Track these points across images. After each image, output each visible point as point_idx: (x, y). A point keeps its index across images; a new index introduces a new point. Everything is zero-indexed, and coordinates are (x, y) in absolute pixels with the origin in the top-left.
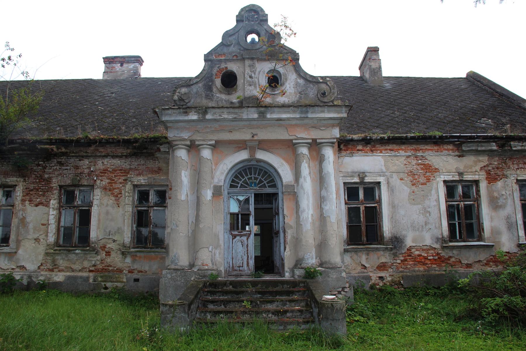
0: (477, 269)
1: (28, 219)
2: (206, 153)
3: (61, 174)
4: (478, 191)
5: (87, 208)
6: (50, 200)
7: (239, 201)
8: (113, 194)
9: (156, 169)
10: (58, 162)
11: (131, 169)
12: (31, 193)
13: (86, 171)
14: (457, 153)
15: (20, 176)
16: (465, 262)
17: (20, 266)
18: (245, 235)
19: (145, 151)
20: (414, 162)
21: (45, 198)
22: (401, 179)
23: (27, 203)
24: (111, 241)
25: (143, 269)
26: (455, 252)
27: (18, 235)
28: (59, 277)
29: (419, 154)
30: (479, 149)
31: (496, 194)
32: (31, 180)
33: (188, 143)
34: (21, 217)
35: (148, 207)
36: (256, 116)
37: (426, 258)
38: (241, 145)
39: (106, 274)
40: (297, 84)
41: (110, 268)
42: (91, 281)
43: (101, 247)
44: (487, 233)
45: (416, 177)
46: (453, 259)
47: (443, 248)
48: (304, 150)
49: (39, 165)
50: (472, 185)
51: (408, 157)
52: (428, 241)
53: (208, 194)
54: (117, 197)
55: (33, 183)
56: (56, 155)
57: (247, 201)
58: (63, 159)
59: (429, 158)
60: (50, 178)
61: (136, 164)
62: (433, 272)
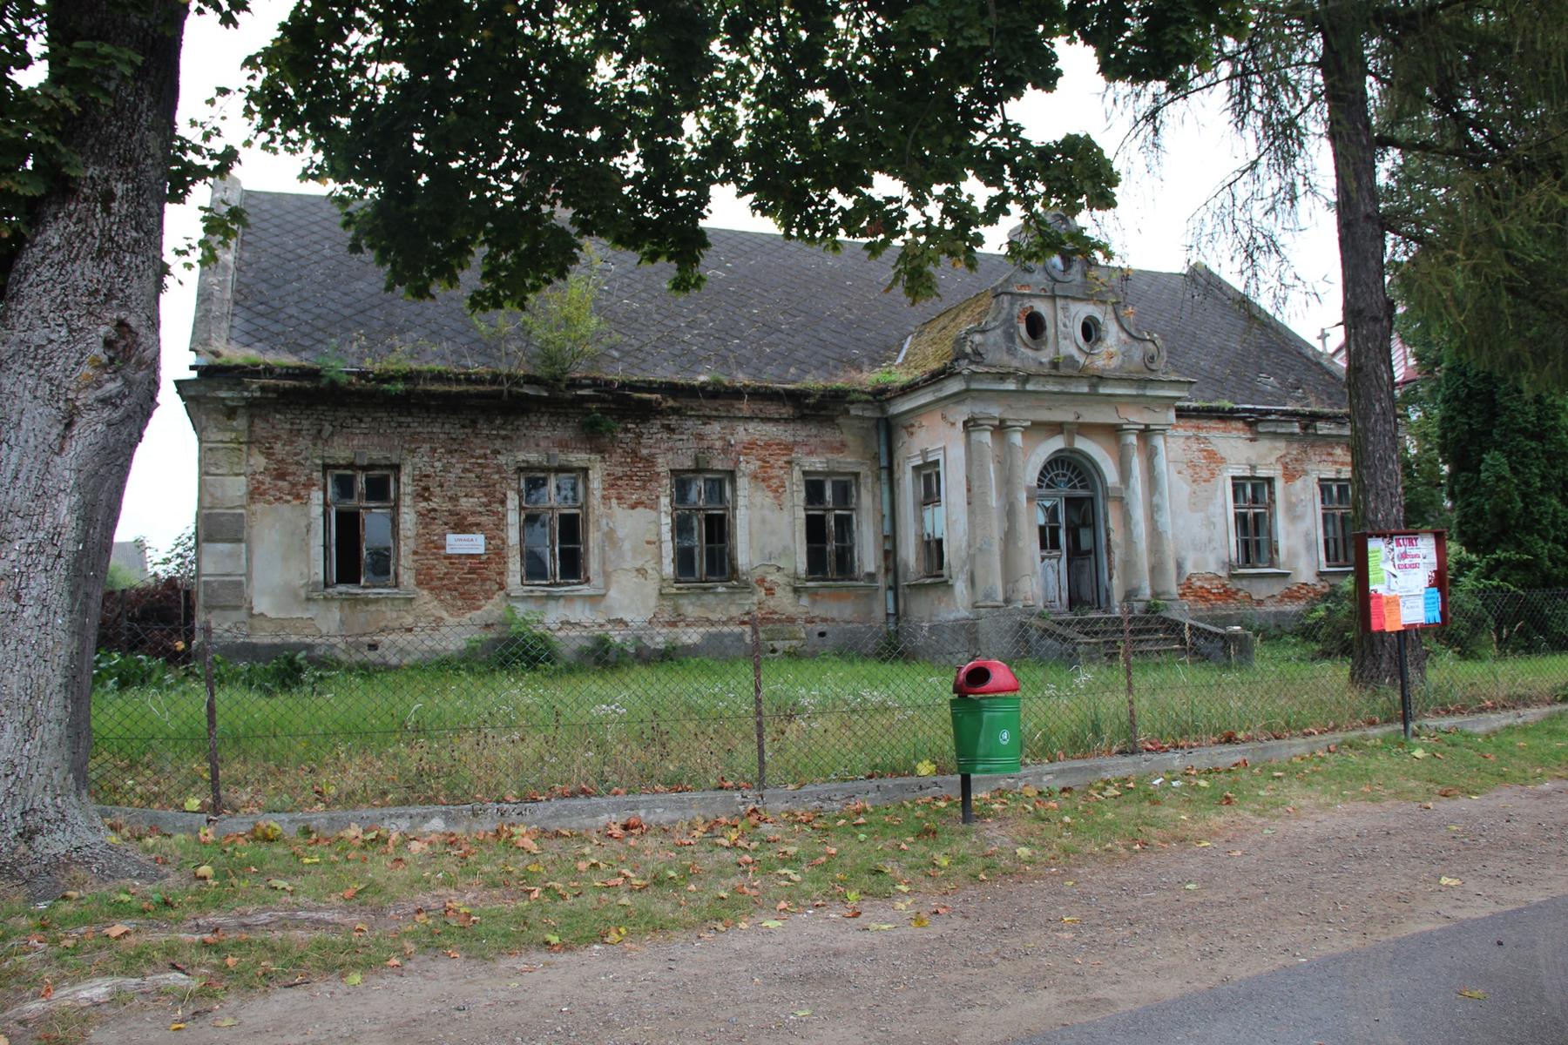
0: (1270, 608)
1: (621, 533)
2: (1017, 438)
3: (671, 449)
4: (1272, 493)
5: (721, 512)
6: (658, 497)
7: (1047, 509)
8: (769, 487)
9: (838, 445)
10: (663, 426)
11: (795, 443)
12: (619, 483)
13: (718, 444)
14: (1249, 436)
15: (592, 451)
16: (1255, 597)
17: (614, 621)
18: (1054, 557)
19: (823, 412)
20: (1195, 447)
21: (647, 493)
22: (1179, 473)
23: (614, 501)
24: (773, 570)
25: (829, 616)
26: (1245, 582)
27: (603, 563)
28: (691, 636)
29: (1203, 434)
30: (1279, 430)
31: (1294, 499)
32: (616, 458)
33: (997, 423)
34: (606, 529)
35: (825, 510)
36: (1086, 390)
37: (1209, 592)
38: (1057, 428)
39: (770, 626)
40: (1119, 339)
41: (776, 617)
42: (748, 639)
43: (757, 582)
44: (1282, 555)
45: (1198, 469)
46: (1242, 594)
47: (1232, 576)
48: (1132, 439)
49: (627, 430)
50: (1263, 485)
51: (1188, 438)
52: (1213, 566)
53: (1023, 496)
54: (777, 492)
55: (621, 463)
56: (662, 413)
57: (1055, 508)
58: (673, 421)
59: (1214, 441)
60: (653, 456)
62: (1218, 612)
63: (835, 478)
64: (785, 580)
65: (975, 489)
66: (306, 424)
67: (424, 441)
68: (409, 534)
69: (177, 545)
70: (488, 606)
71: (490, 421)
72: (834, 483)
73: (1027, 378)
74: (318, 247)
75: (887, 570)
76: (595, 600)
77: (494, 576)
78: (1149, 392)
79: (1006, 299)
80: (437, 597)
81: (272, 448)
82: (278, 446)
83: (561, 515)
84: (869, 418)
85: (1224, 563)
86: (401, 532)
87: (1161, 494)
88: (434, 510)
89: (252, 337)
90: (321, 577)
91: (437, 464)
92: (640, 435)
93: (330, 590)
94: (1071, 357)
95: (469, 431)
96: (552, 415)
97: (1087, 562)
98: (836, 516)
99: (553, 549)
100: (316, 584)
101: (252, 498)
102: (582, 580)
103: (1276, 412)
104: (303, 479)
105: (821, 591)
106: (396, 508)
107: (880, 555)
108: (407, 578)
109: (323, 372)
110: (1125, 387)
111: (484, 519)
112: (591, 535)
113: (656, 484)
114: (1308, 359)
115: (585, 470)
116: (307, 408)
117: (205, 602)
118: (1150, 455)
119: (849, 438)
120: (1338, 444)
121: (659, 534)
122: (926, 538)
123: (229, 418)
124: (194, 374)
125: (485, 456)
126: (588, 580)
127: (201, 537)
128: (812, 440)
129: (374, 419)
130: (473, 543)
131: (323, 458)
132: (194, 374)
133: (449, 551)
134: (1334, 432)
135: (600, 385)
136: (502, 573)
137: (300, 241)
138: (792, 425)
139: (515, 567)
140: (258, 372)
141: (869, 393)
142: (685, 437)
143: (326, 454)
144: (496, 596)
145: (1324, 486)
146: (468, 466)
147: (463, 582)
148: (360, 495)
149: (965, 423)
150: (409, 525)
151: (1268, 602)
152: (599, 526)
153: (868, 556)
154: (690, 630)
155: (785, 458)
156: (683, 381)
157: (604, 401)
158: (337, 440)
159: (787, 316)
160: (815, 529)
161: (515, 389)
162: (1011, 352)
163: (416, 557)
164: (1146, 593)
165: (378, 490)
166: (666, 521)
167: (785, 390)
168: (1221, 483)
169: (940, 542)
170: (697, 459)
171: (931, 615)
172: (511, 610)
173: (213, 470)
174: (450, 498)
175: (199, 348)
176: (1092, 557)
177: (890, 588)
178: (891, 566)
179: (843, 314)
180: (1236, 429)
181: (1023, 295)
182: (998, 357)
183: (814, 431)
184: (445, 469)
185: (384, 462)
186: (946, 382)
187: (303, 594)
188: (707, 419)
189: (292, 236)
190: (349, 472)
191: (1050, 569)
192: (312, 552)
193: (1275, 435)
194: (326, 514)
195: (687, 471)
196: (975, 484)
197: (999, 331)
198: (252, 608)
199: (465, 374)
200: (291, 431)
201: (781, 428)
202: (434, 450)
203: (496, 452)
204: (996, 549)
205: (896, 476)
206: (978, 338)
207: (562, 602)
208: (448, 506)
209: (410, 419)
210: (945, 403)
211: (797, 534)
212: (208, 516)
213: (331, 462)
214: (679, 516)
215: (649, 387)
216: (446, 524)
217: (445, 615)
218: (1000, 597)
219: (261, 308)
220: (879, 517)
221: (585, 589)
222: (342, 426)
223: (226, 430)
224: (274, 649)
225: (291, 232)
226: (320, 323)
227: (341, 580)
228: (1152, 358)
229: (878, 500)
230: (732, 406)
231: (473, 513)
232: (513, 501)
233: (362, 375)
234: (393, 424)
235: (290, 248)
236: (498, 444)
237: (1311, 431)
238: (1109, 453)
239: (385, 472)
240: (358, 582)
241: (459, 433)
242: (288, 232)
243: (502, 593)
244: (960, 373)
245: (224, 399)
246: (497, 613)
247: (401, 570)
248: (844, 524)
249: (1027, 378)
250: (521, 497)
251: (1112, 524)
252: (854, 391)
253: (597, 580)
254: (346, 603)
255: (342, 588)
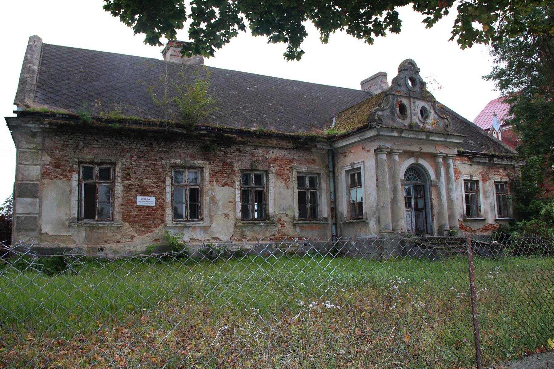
1: (218, 197)
3: (240, 160)
4: (478, 187)
5: (261, 189)
6: (234, 182)
7: (406, 190)
8: (283, 178)
9: (311, 161)
10: (237, 149)
11: (294, 159)
12: (217, 174)
13: (261, 158)
15: (205, 159)
16: (473, 229)
19: (306, 146)
21: (230, 179)
23: (215, 183)
24: (284, 215)
26: (469, 223)
27: (210, 211)
28: (249, 245)
30: (481, 161)
31: (486, 189)
32: (216, 163)
33: (389, 150)
34: (211, 195)
35: (306, 189)
36: (424, 137)
38: (411, 154)
40: (434, 117)
43: (277, 221)
46: (468, 228)
47: (466, 221)
48: (441, 160)
49: (221, 151)
50: (474, 183)
53: (399, 183)
54: (286, 180)
57: (410, 189)
58: (241, 147)
60: (232, 163)
61: (297, 155)
63: (310, 175)
64: (290, 220)
65: (380, 180)
66: (71, 142)
67: (127, 152)
68: (119, 196)
69: (7, 202)
70: (156, 231)
71: (159, 144)
72: (310, 177)
73: (401, 131)
74: (77, 67)
75: (332, 216)
76: (206, 229)
77: (159, 216)
78: (448, 140)
79: (391, 96)
80: (132, 226)
81: (54, 153)
82: (57, 152)
83: (190, 188)
84: (325, 149)
85: (461, 215)
86: (116, 195)
87: (452, 184)
88: (132, 185)
89: (44, 101)
90: (76, 216)
91: (133, 163)
92: (226, 153)
93: (80, 222)
94: (417, 123)
95: (149, 148)
96: (187, 143)
97: (421, 213)
98: (311, 192)
99: (187, 205)
100: (73, 219)
101: (43, 176)
102: (200, 219)
103: (479, 154)
104: (68, 168)
105: (305, 225)
106: (114, 183)
107: (329, 210)
108: (118, 217)
109: (80, 117)
110: (439, 137)
111: (155, 189)
112: (204, 198)
113: (233, 176)
114: (482, 135)
115: (202, 168)
116: (72, 134)
117: (17, 227)
118: (447, 168)
119: (316, 158)
120: (501, 168)
121: (235, 199)
122: (352, 202)
123: (33, 137)
124: (15, 115)
125: (156, 160)
126: (202, 219)
127: (16, 195)
128: (301, 158)
129: (104, 141)
130: (150, 201)
131: (78, 158)
132: (15, 115)
133: (138, 204)
134: (500, 163)
135: (209, 130)
136: (163, 215)
137: (69, 65)
138: (292, 151)
139: (169, 212)
140: (48, 116)
141: (326, 138)
142: (246, 155)
143: (80, 157)
144: (160, 226)
145: (496, 183)
146: (148, 164)
147: (145, 219)
148: (96, 176)
149: (375, 150)
150: (119, 192)
151: (478, 231)
152: (208, 194)
153: (324, 210)
154: (250, 243)
155: (289, 166)
156: (246, 130)
157: (211, 136)
158: (86, 150)
159: (283, 107)
160: (302, 197)
161: (171, 129)
162: (393, 120)
163: (122, 207)
164: (447, 227)
165: (105, 175)
166: (238, 192)
167: (290, 135)
168: (460, 182)
169: (360, 204)
170: (252, 164)
171: (355, 236)
172: (167, 232)
173: (23, 162)
174: (139, 179)
175: (18, 103)
176: (424, 211)
177: (334, 224)
178: (334, 215)
179: (305, 108)
180: (465, 160)
181: (398, 96)
182: (388, 122)
183: (302, 154)
184: (137, 166)
185: (108, 161)
186: (367, 132)
187: (67, 223)
188: (256, 147)
189: (65, 63)
190: (91, 166)
191: (408, 216)
192: (72, 203)
193: (479, 163)
194: (79, 185)
195: (248, 170)
196: (380, 177)
197: (388, 111)
198: (41, 230)
199: (148, 121)
200: (63, 145)
201: (288, 152)
202: (132, 157)
203: (161, 159)
204: (389, 206)
205: (336, 175)
206: (380, 113)
207: (191, 229)
208: (138, 183)
209: (121, 142)
210: (364, 142)
211: (295, 200)
212: (20, 185)
213: (83, 160)
214: (243, 191)
215: (231, 131)
216: (137, 191)
217: (136, 234)
218: (391, 229)
219: (50, 90)
220: (329, 193)
221: (201, 224)
222: (88, 144)
223: (31, 143)
224: (52, 250)
225: (65, 61)
226: (79, 98)
227: (86, 217)
228: (447, 126)
229: (328, 185)
230: (267, 141)
231: (150, 187)
232: (168, 181)
233: (99, 119)
234: (113, 144)
235: (65, 67)
236: (162, 155)
237: (492, 162)
238: (432, 166)
239: (109, 166)
240: (95, 218)
241: (144, 149)
242: (63, 61)
243: (163, 224)
244: (375, 127)
245: (30, 128)
246: (160, 234)
247: (115, 213)
248: (314, 195)
249: (401, 131)
250: (172, 180)
251: (433, 197)
252: (319, 137)
253: (207, 220)
254: (88, 229)
255: (86, 221)
